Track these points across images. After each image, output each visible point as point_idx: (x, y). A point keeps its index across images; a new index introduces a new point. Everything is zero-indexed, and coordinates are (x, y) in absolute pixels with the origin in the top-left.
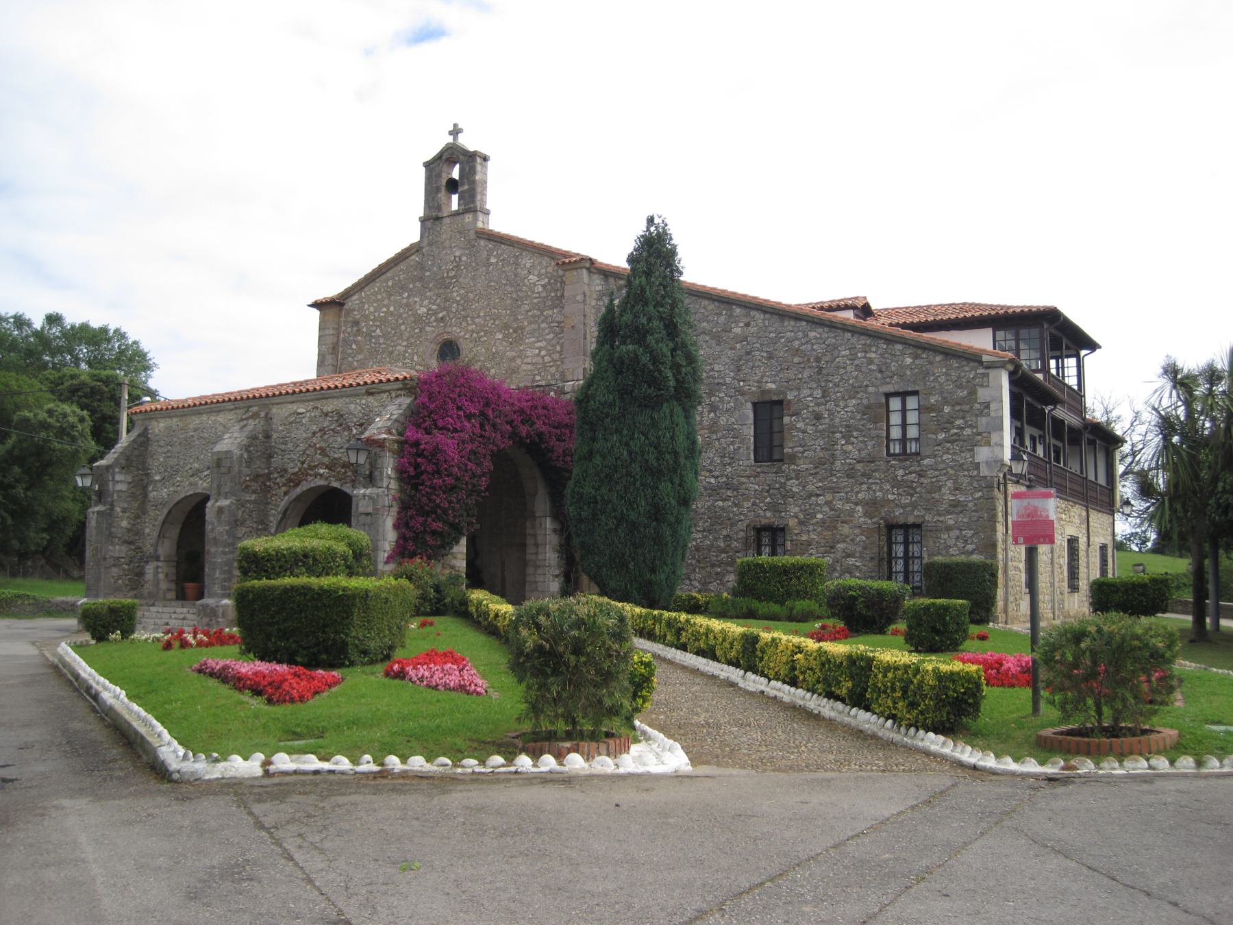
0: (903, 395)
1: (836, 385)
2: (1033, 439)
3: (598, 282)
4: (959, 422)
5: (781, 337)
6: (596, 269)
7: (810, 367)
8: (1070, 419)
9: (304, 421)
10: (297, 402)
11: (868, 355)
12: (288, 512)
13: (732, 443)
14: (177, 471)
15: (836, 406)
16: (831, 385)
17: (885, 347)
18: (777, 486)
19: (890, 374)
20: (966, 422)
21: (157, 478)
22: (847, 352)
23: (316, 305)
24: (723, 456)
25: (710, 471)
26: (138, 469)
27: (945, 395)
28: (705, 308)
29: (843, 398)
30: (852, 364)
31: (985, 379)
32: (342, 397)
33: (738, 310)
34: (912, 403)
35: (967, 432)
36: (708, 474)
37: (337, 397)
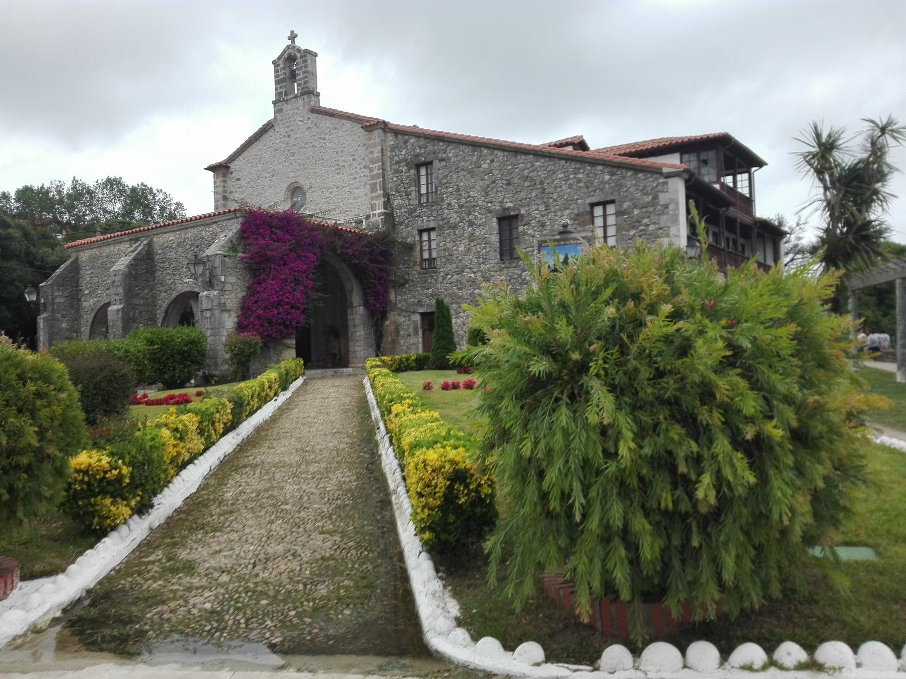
0: (604, 204)
1: (555, 200)
2: (743, 246)
3: (391, 138)
4: (646, 221)
5: (516, 168)
6: (389, 129)
7: (537, 189)
8: (741, 216)
9: (174, 246)
10: (168, 232)
11: (578, 176)
12: (169, 312)
13: (485, 248)
14: (98, 286)
15: (556, 216)
16: (551, 201)
17: (590, 168)
18: (516, 276)
19: (594, 189)
20: (651, 220)
21: (86, 292)
22: (562, 175)
23: (211, 168)
24: (479, 258)
25: (471, 269)
26: (72, 287)
27: (635, 201)
28: (463, 151)
29: (560, 210)
30: (566, 184)
31: (665, 186)
32: (197, 226)
33: (485, 151)
34: (611, 209)
35: (652, 228)
36: (469, 271)
37: (193, 227)
